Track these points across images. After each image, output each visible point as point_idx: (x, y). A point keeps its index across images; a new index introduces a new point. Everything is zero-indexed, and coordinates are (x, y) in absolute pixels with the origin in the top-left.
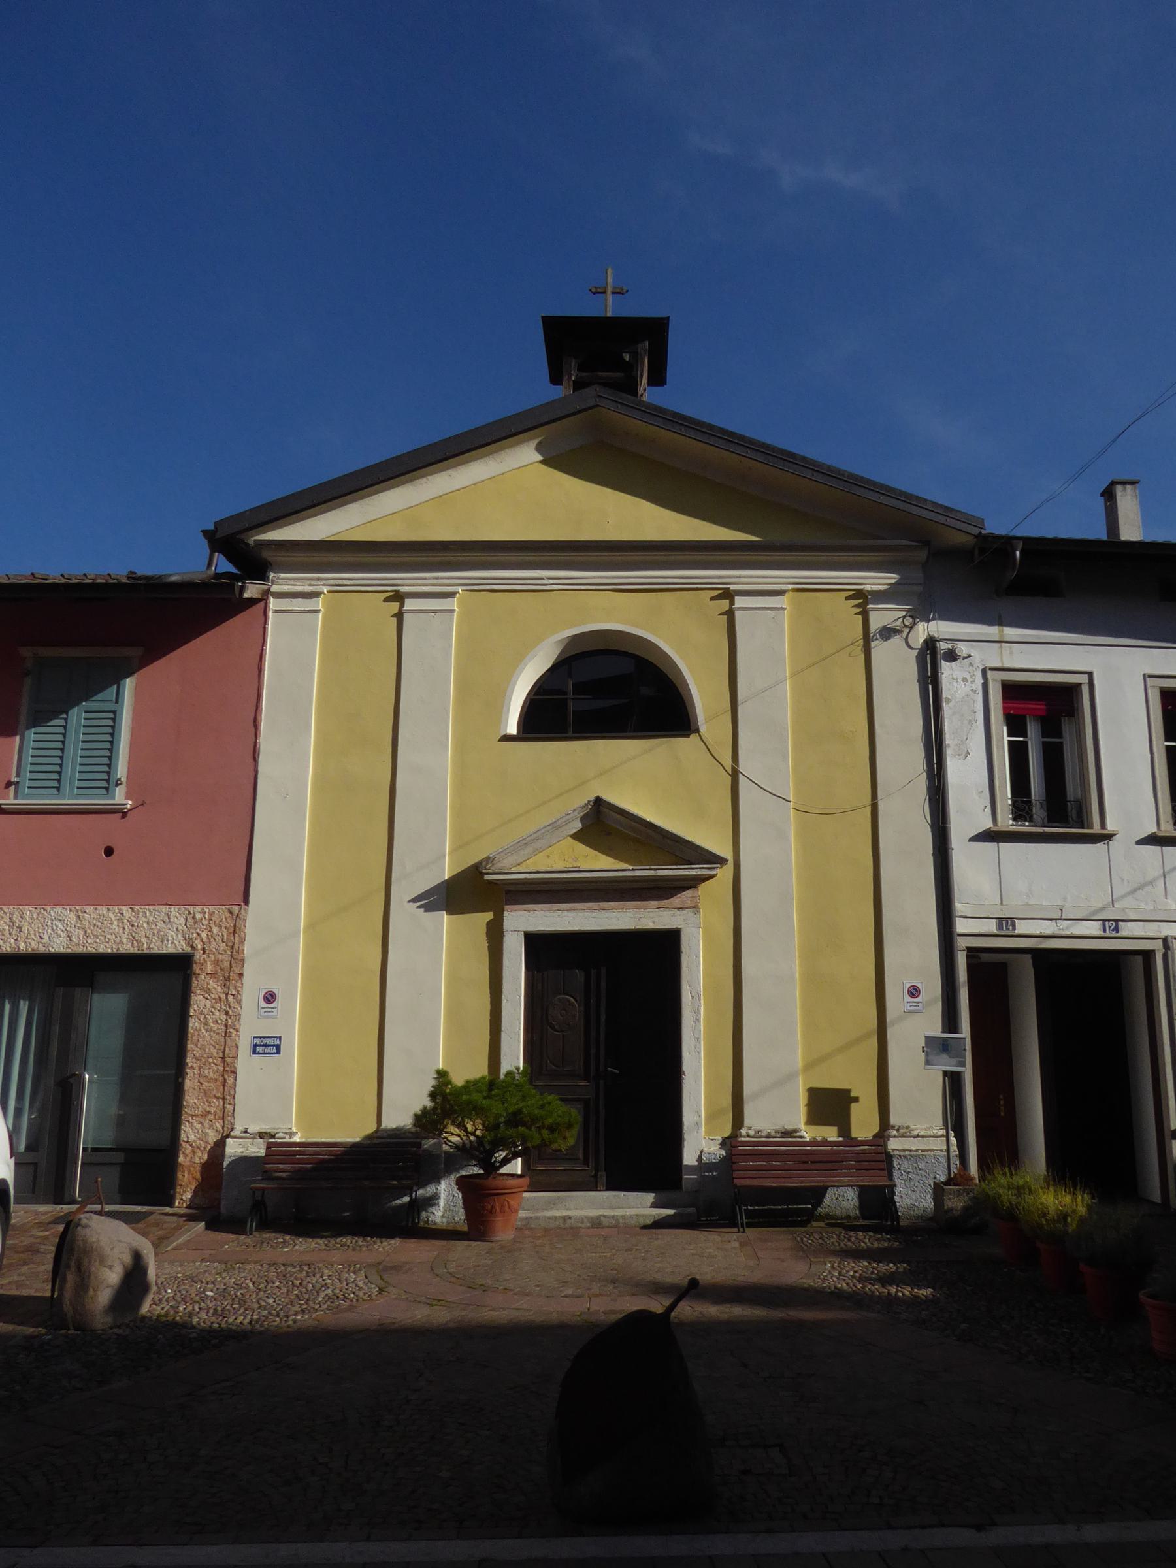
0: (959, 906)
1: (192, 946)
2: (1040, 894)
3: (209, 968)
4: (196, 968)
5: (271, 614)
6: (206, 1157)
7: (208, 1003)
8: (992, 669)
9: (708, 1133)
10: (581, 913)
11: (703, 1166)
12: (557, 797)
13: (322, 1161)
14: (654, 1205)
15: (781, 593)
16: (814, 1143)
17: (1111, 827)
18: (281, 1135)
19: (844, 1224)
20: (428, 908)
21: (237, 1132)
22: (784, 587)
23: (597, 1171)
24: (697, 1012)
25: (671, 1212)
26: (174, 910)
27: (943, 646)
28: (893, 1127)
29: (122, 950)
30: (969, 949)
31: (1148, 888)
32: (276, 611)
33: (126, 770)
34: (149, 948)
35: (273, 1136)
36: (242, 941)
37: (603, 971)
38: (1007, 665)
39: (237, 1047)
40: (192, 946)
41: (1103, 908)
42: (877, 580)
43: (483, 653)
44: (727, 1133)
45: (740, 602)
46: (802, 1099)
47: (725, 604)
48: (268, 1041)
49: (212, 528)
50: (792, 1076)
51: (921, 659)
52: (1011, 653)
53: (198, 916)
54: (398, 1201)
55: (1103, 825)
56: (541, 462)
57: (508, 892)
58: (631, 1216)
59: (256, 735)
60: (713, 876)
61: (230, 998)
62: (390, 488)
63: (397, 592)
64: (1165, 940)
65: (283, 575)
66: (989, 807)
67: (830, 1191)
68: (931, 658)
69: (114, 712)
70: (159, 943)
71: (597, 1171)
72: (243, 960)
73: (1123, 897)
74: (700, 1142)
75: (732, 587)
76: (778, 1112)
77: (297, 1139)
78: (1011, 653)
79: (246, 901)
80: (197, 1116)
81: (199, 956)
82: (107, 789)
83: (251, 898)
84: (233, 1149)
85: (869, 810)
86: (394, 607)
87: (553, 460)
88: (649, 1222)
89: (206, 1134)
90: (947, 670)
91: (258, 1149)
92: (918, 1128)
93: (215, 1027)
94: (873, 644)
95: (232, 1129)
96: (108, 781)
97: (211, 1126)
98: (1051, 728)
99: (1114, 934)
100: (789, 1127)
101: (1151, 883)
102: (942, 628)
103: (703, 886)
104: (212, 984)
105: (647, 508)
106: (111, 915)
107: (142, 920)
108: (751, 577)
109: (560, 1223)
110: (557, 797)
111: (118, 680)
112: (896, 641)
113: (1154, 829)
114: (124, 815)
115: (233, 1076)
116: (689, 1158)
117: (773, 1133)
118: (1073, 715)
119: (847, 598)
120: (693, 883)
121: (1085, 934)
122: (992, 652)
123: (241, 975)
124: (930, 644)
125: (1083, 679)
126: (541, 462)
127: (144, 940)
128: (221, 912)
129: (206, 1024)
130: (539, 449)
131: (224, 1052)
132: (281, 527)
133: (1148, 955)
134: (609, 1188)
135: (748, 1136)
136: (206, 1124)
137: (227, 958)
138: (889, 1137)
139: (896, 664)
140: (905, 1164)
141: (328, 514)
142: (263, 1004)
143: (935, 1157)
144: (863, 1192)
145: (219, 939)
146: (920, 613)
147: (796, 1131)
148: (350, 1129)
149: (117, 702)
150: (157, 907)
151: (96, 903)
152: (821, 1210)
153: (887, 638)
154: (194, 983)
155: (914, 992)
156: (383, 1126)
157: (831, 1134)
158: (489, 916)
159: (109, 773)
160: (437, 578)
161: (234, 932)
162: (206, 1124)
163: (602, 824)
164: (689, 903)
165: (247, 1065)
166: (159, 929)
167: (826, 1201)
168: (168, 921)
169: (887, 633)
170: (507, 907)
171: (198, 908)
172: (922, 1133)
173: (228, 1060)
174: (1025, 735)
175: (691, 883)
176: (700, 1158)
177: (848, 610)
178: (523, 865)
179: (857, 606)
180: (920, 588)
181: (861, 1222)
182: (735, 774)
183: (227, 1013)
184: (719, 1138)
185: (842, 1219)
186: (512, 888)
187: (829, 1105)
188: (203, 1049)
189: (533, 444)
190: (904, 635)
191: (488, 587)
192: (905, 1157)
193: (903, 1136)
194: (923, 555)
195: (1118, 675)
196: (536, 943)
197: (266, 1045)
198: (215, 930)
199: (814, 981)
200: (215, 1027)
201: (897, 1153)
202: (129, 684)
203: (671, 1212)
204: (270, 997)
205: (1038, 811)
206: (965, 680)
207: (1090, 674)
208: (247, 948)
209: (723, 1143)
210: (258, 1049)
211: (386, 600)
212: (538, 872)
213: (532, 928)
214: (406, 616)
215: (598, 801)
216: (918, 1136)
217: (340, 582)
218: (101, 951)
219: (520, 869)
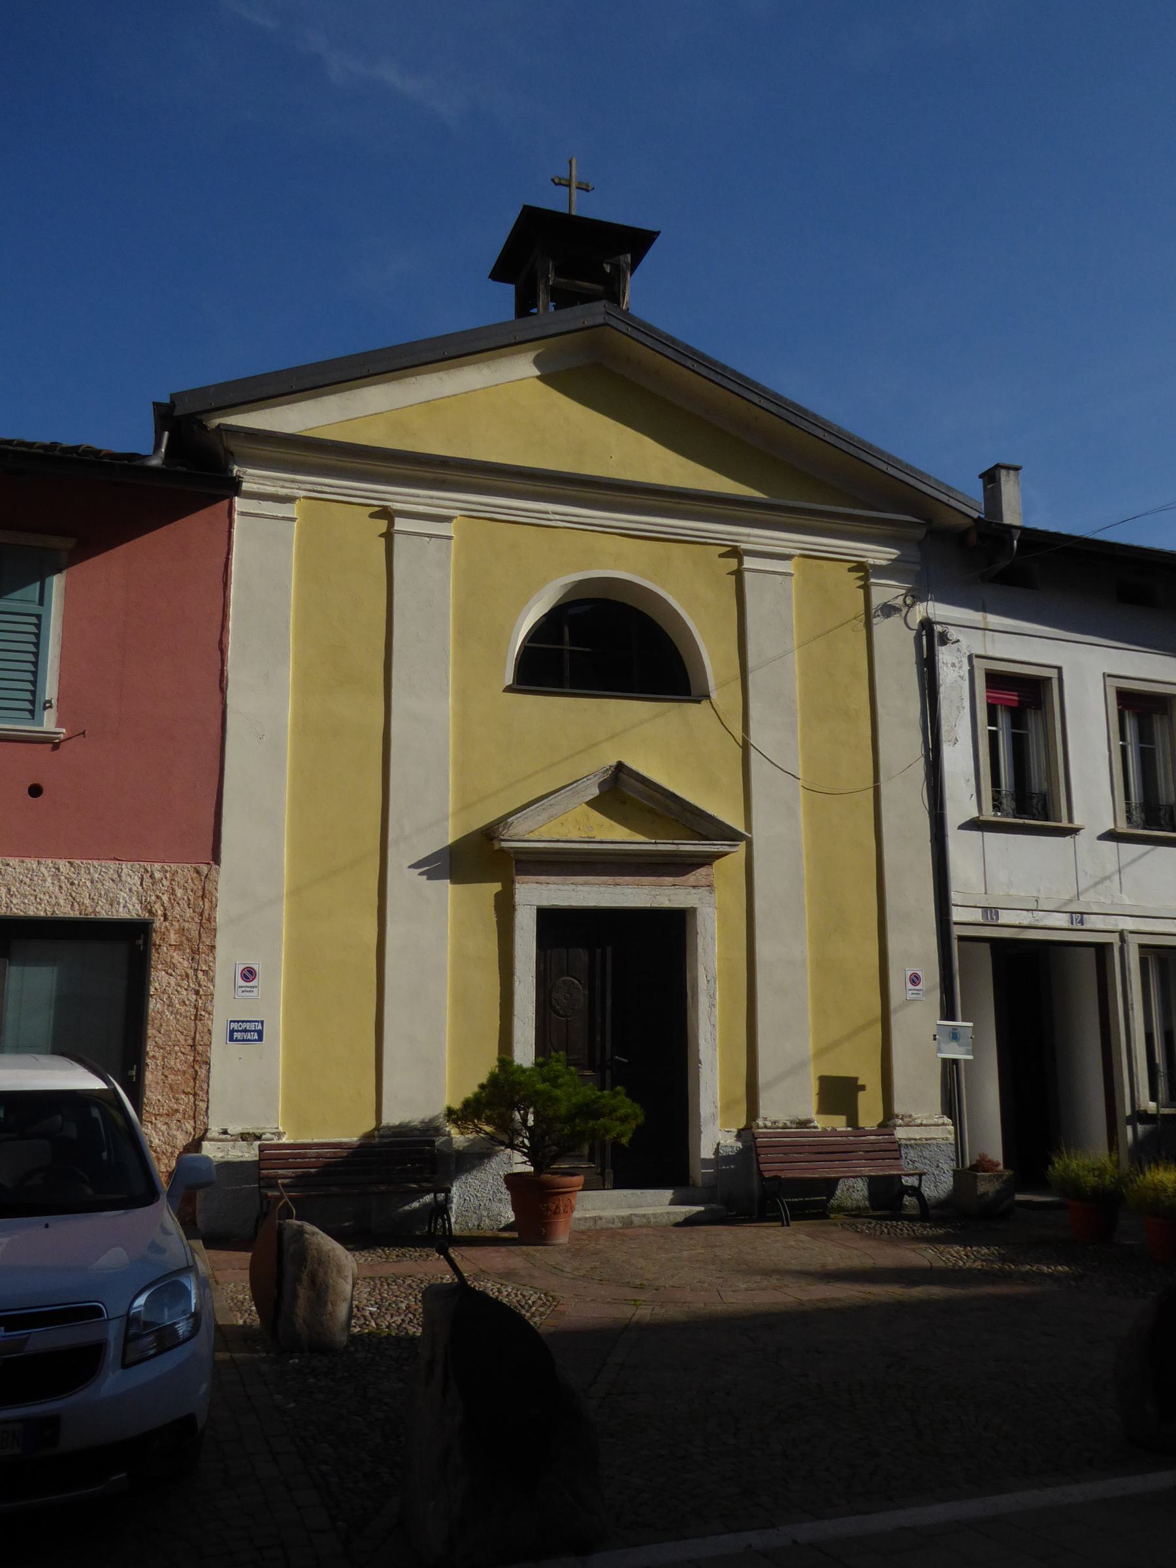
0: (955, 897)
1: (150, 912)
2: (1018, 883)
3: (173, 938)
4: (156, 938)
5: (236, 516)
6: (174, 1164)
7: (173, 981)
8: (978, 656)
9: (723, 1125)
10: (595, 888)
11: (720, 1158)
12: (566, 759)
13: (328, 1165)
14: (673, 1203)
15: (788, 557)
16: (824, 1133)
17: (1077, 822)
18: (268, 1136)
19: (855, 1213)
20: (432, 875)
21: (214, 1131)
22: (793, 552)
23: (603, 1168)
24: (713, 997)
25: (702, 1208)
26: (126, 868)
27: (938, 628)
28: (897, 1116)
29: (59, 913)
30: (1141, 946)
31: (1107, 883)
32: (243, 514)
33: (56, 690)
34: (94, 911)
35: (258, 1138)
36: (214, 907)
37: (609, 949)
38: (990, 653)
39: (210, 1032)
40: (150, 912)
41: (1070, 901)
42: (879, 555)
43: (471, 585)
44: (742, 1123)
45: (400, 524)
46: (813, 1087)
47: (733, 563)
48: (248, 1026)
49: (167, 401)
50: (803, 1065)
51: (918, 639)
52: (993, 641)
53: (157, 875)
54: (407, 1208)
55: (1071, 820)
56: (538, 377)
57: (518, 862)
58: (662, 1214)
59: (223, 661)
60: (726, 854)
61: (200, 974)
62: (375, 384)
63: (385, 508)
64: (1121, 933)
65: (250, 471)
66: (974, 798)
67: (840, 1182)
68: (929, 638)
69: (39, 617)
70: (107, 907)
71: (603, 1168)
72: (215, 930)
73: (1087, 890)
74: (715, 1134)
75: (743, 546)
76: (791, 1102)
77: (285, 1140)
78: (993, 641)
79: (216, 857)
80: (162, 1115)
81: (158, 923)
82: (32, 712)
83: (224, 856)
84: (210, 1150)
85: (871, 791)
86: (382, 525)
87: (555, 377)
88: (680, 1219)
89: (174, 1137)
90: (944, 655)
91: (248, 1153)
92: (920, 1116)
93: (182, 1009)
94: (875, 621)
95: (206, 1130)
96: (33, 702)
97: (179, 1128)
98: (1018, 719)
99: (1079, 927)
100: (803, 1117)
101: (1108, 878)
102: (940, 611)
103: (717, 863)
104: (177, 957)
105: (649, 446)
106: (43, 869)
107: (84, 877)
108: (401, 494)
109: (590, 1224)
110: (566, 759)
111: (41, 572)
112: (896, 619)
113: (976, 814)
114: (56, 746)
115: (205, 1067)
116: (707, 1152)
117: (788, 1124)
118: (1040, 709)
119: (850, 570)
120: (707, 860)
121: (1054, 924)
122: (985, 638)
123: (212, 948)
124: (927, 625)
125: (1053, 674)
126: (538, 377)
127: (87, 901)
128: (185, 871)
129: (171, 1005)
130: (537, 362)
131: (194, 1039)
132: (249, 411)
133: (1102, 950)
134: (616, 1186)
135: (766, 1127)
136: (173, 1125)
137: (194, 928)
138: (895, 1126)
139: (895, 641)
140: (912, 1154)
141: (303, 404)
142: (240, 982)
143: (938, 1146)
144: (872, 1181)
145: (184, 904)
146: (917, 595)
147: (810, 1121)
148: (346, 1128)
149: (41, 603)
150: (103, 863)
151: (23, 852)
152: (834, 1202)
153: (888, 616)
154: (154, 956)
155: (915, 979)
156: (384, 1122)
157: (839, 1123)
158: (497, 887)
159: (33, 693)
160: (432, 498)
161: (203, 897)
162: (173, 1125)
163: (621, 792)
164: (703, 881)
165: (221, 1053)
166: (111, 889)
167: (838, 1192)
168: (118, 879)
169: (888, 610)
170: (518, 878)
171: (157, 866)
172: (924, 1122)
173: (200, 1048)
174: (996, 725)
175: (701, 860)
176: (717, 1151)
177: (852, 581)
178: (536, 833)
179: (859, 578)
180: (918, 568)
181: (871, 1213)
182: (746, 746)
183: (197, 993)
184: (735, 1130)
185: (852, 1210)
186: (523, 857)
187: (838, 1094)
188: (168, 1034)
189: (532, 355)
190: (903, 613)
191: (488, 515)
192: (911, 1146)
193: (908, 1125)
194: (921, 533)
195: (1089, 672)
196: (548, 918)
197: (245, 1031)
198: (179, 893)
199: (824, 967)
200: (182, 1009)
201: (903, 1142)
202: (57, 583)
203: (702, 1208)
204: (249, 974)
205: (1008, 803)
206: (953, 665)
207: (1060, 669)
208: (220, 916)
209: (740, 1135)
210: (236, 1035)
211: (373, 516)
212: (558, 841)
213: (545, 903)
214: (398, 539)
215: (620, 766)
216: (921, 1125)
217: (319, 488)
218: (31, 913)
219: (526, 837)
